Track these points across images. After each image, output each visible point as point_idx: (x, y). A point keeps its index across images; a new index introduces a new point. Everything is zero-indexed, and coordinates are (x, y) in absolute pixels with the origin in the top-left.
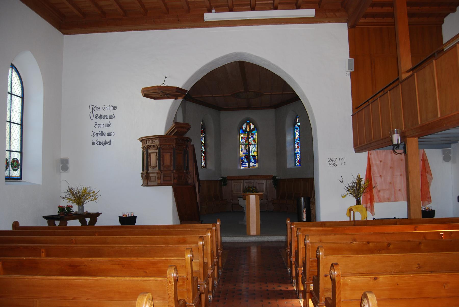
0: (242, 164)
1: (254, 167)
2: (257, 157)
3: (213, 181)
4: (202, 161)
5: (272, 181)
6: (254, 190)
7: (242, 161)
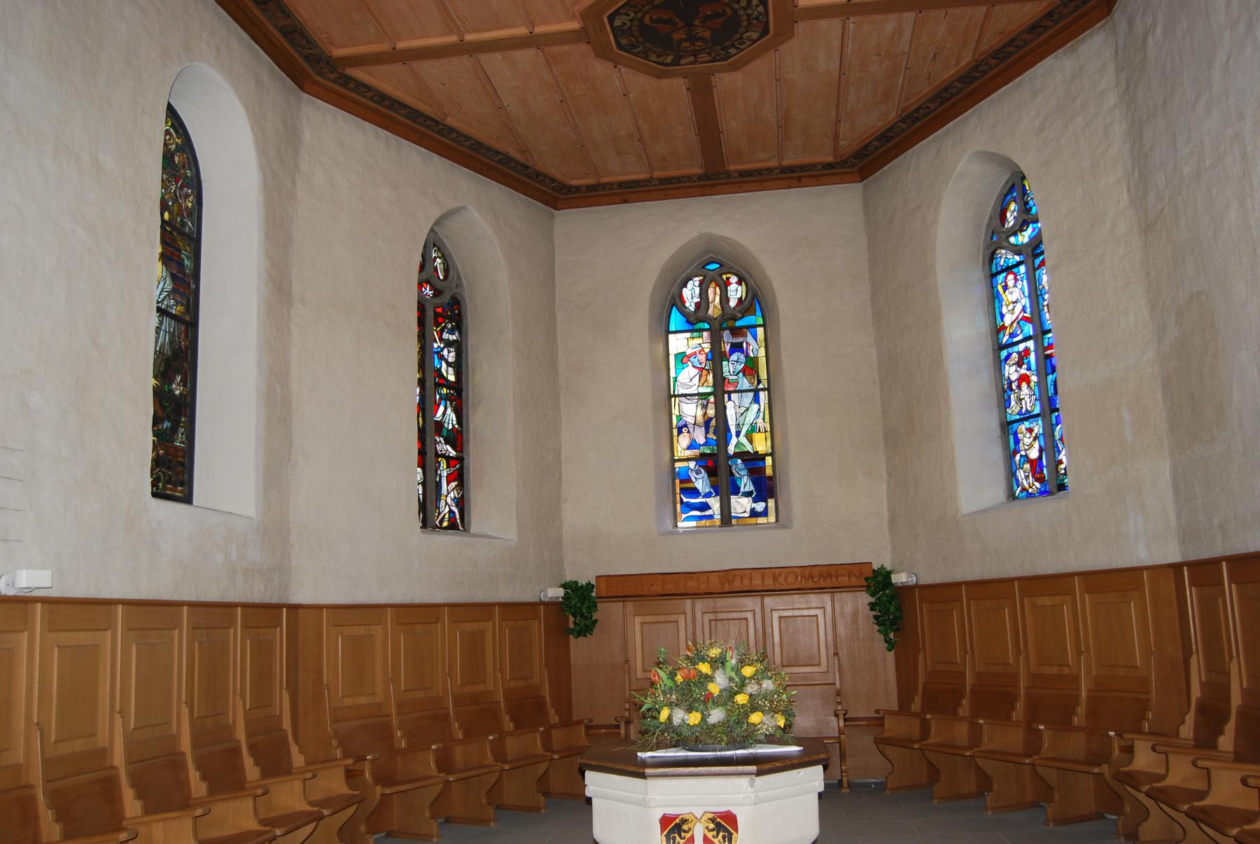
1: (753, 520)
2: (769, 460)
3: (504, 606)
4: (439, 485)
6: (752, 688)
7: (683, 490)
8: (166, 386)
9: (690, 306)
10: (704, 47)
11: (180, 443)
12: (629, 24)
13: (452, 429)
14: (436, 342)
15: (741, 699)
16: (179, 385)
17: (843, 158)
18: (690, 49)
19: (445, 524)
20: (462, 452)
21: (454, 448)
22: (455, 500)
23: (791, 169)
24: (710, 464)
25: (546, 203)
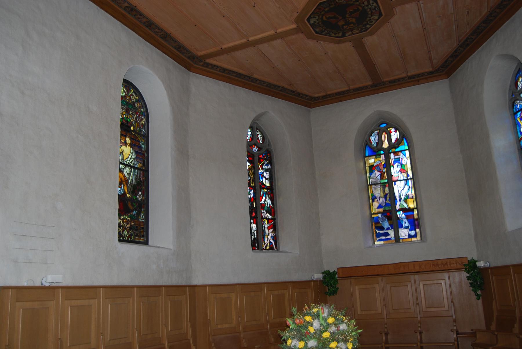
0: (378, 235)
1: (410, 240)
2: (416, 212)
3: (168, 287)
4: (264, 231)
5: (465, 275)
8: (134, 197)
9: (374, 144)
10: (354, 26)
11: (142, 219)
12: (317, 21)
13: (269, 207)
14: (260, 170)
15: (326, 335)
16: (140, 196)
17: (437, 69)
18: (348, 28)
19: (268, 248)
20: (274, 216)
21: (270, 215)
22: (272, 237)
23: (413, 77)
24: (388, 214)
25: (306, 106)
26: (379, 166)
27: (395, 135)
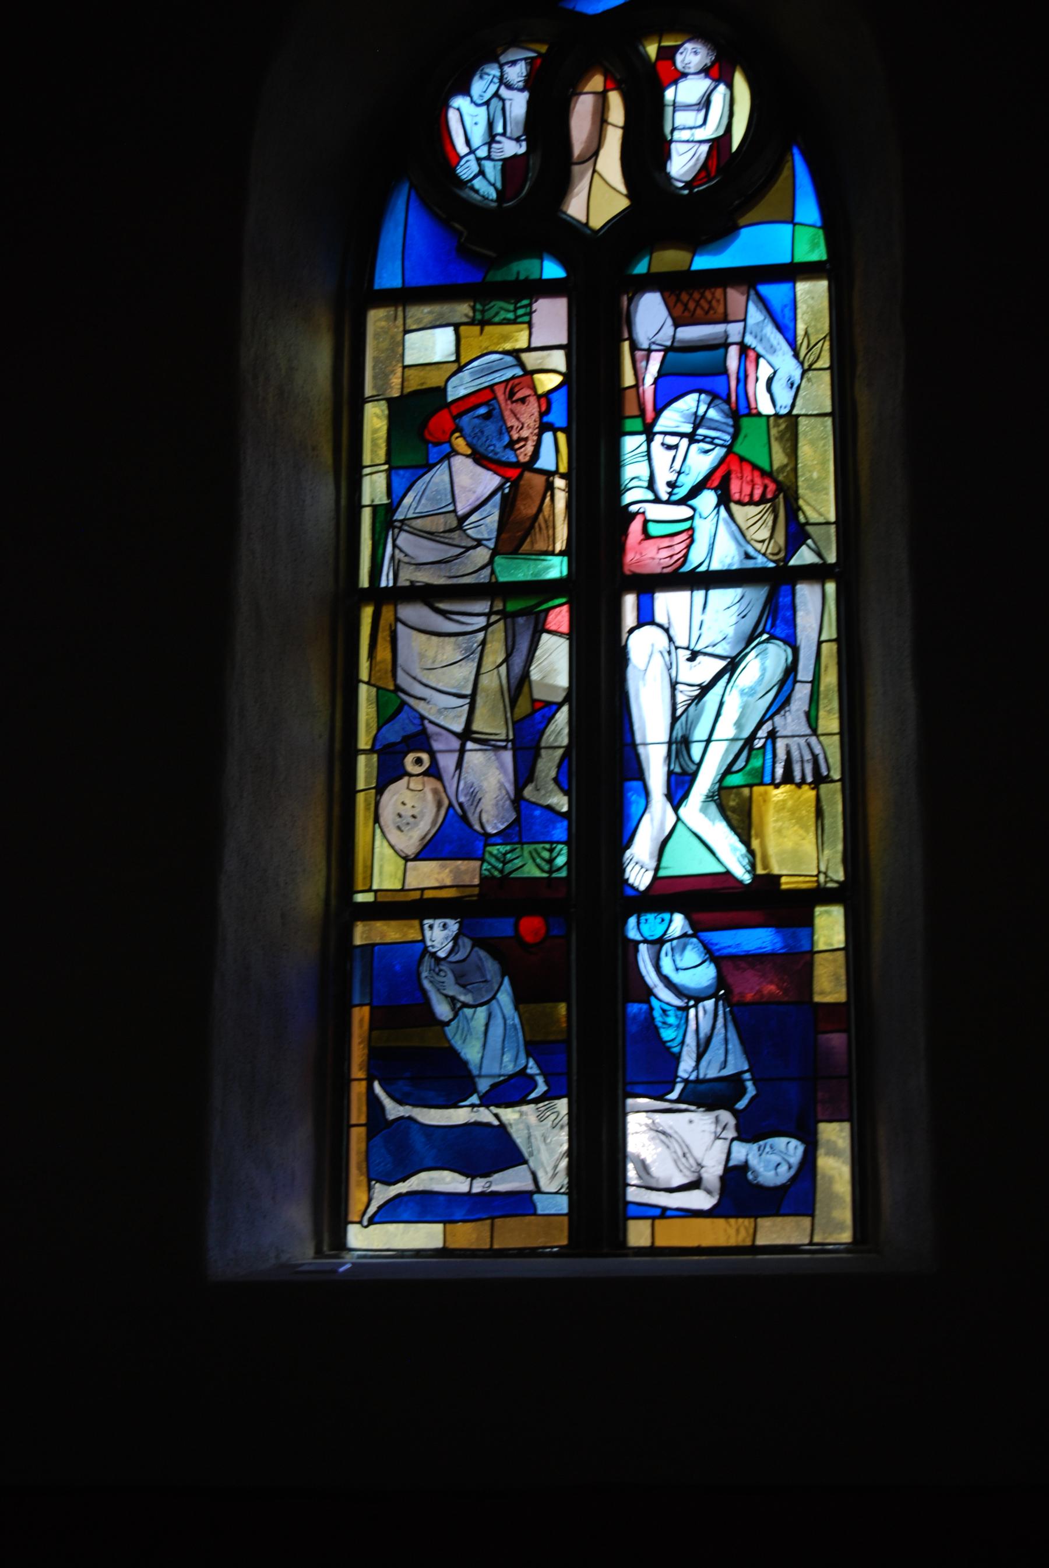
26: (507, 407)
27: (706, 103)
